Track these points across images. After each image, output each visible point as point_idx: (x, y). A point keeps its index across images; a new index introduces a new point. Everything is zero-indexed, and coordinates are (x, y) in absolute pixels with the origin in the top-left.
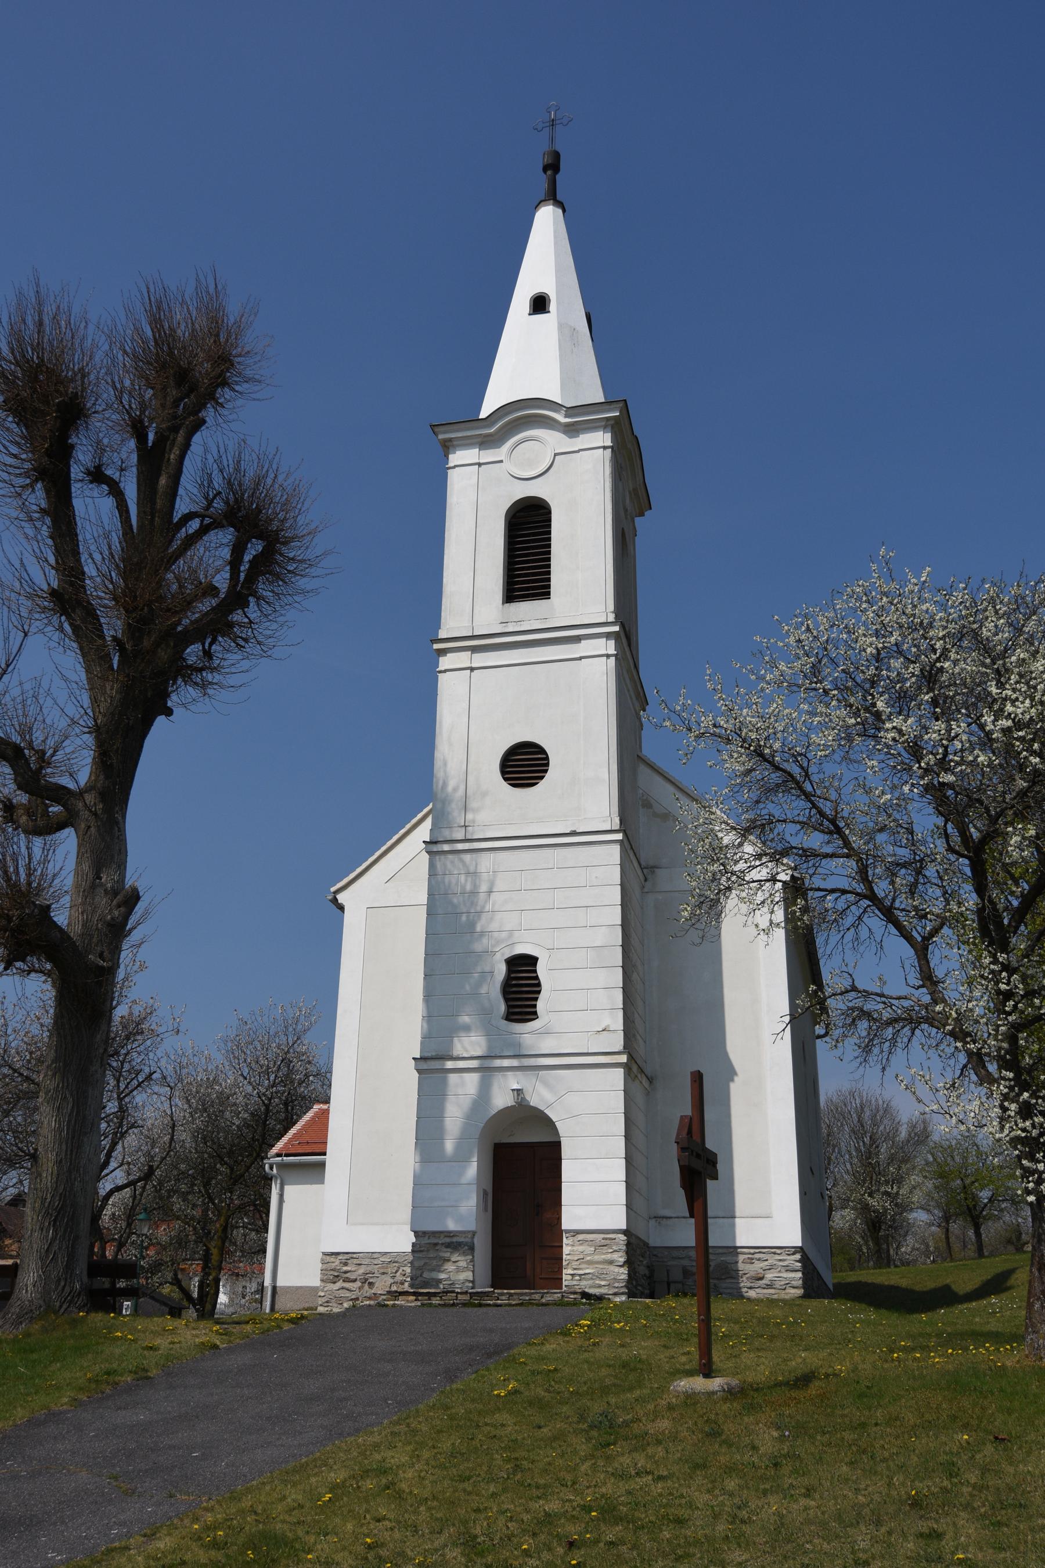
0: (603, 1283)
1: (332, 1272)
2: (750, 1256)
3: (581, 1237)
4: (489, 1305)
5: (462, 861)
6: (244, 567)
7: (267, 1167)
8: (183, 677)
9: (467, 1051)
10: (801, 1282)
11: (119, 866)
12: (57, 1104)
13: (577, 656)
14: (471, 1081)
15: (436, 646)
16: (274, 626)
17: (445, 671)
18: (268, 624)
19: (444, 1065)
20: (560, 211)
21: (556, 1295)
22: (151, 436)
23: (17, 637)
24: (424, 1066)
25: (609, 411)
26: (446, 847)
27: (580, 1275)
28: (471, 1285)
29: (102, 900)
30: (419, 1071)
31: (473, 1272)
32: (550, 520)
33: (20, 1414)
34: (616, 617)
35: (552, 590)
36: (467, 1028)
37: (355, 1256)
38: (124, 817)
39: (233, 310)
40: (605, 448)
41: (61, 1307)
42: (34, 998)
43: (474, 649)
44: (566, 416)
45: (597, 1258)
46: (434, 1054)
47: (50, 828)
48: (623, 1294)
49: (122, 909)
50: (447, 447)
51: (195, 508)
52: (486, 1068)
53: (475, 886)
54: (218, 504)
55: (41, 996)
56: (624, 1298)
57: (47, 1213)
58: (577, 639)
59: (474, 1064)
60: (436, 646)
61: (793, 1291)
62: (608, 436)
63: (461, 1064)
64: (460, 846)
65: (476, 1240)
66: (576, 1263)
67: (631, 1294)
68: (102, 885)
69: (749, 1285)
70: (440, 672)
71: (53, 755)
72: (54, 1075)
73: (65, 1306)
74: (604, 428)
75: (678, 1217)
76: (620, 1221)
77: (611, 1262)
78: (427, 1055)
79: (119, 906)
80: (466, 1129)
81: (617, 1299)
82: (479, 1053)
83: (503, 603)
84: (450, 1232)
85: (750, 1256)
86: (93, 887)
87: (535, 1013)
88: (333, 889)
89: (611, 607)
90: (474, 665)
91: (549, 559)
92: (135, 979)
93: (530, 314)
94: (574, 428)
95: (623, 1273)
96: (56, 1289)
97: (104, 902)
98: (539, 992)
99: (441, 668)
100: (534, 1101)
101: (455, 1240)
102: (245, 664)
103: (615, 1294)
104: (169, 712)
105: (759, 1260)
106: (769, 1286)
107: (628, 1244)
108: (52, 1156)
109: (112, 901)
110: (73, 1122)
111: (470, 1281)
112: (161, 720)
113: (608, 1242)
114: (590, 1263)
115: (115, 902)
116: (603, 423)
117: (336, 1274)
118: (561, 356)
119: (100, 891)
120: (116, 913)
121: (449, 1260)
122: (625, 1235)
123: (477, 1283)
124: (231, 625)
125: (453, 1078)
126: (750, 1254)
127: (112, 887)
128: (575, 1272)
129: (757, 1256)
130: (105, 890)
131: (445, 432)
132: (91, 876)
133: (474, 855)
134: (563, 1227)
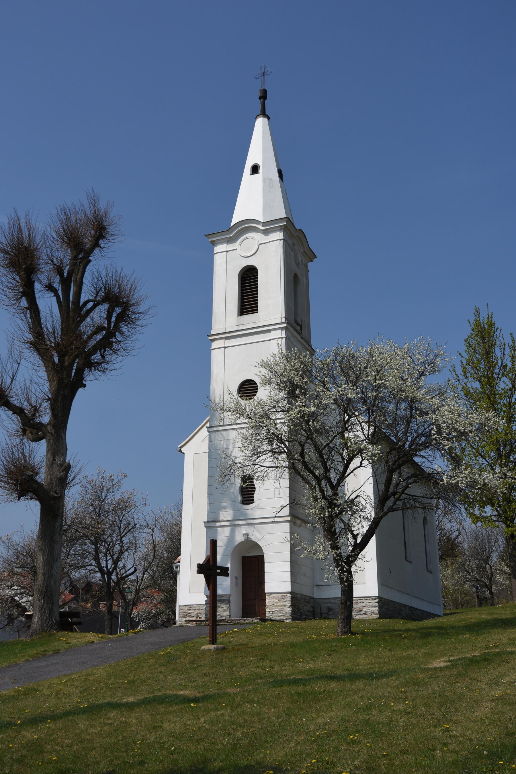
0: (281, 615)
1: (184, 613)
2: (356, 601)
3: (273, 595)
4: (222, 625)
5: (222, 434)
6: (113, 319)
7: (174, 567)
8: (94, 367)
9: (225, 518)
10: (378, 612)
11: (63, 455)
12: (42, 551)
13: (269, 339)
14: (227, 530)
15: (210, 338)
16: (130, 342)
17: (214, 349)
18: (127, 341)
19: (216, 524)
20: (266, 120)
21: (250, 620)
22: (65, 275)
23: (16, 365)
24: (208, 525)
25: (281, 222)
26: (215, 429)
27: (272, 612)
28: (229, 617)
29: (56, 469)
30: (206, 527)
31: (230, 611)
32: (257, 275)
33: (5, 664)
34: (286, 320)
35: (258, 308)
36: (225, 508)
37: (193, 606)
38: (65, 434)
39: (102, 206)
40: (280, 240)
41: (47, 629)
42: (77, 494)
43: (226, 338)
44: (263, 226)
45: (279, 604)
46: (212, 520)
47: (38, 439)
48: (290, 619)
49: (64, 472)
50: (214, 244)
51: (91, 298)
52: (233, 525)
53: (227, 445)
54: (102, 294)
55: (81, 493)
56: (290, 620)
57: (41, 594)
58: (269, 331)
59: (227, 523)
60: (210, 338)
61: (374, 616)
62: (282, 234)
63: (223, 524)
64: (221, 428)
65: (231, 598)
66: (271, 606)
67: (293, 619)
68: (56, 463)
69: (356, 613)
70: (212, 349)
71: (39, 408)
72: (41, 540)
73: (49, 629)
74: (280, 230)
75: (326, 585)
76: (288, 588)
77: (285, 606)
78: (210, 520)
79: (63, 471)
80: (225, 550)
81: (288, 621)
82: (230, 519)
83: (238, 316)
84: (220, 595)
85: (356, 601)
86: (52, 464)
87: (253, 500)
88: (179, 446)
89: (283, 315)
90: (226, 346)
91: (257, 294)
92: (122, 482)
93: (251, 175)
94: (266, 231)
95: (290, 610)
96: (46, 622)
97: (57, 470)
98: (255, 491)
99: (212, 348)
100: (253, 538)
101: (222, 598)
102: (120, 359)
103: (287, 619)
104: (84, 386)
105: (360, 602)
106: (365, 614)
107: (292, 598)
108: (41, 572)
109: (60, 469)
110: (49, 558)
111: (228, 615)
112: (81, 390)
113: (284, 597)
114: (277, 606)
115: (61, 470)
116: (279, 228)
117: (186, 614)
118: (263, 195)
119: (55, 465)
120: (62, 474)
121: (220, 607)
122: (291, 594)
123: (231, 616)
124: (111, 343)
125: (220, 530)
126: (356, 600)
127: (60, 463)
128: (271, 610)
129: (359, 601)
130: (57, 465)
131: (211, 238)
132: (51, 460)
133: (227, 432)
134: (266, 592)
